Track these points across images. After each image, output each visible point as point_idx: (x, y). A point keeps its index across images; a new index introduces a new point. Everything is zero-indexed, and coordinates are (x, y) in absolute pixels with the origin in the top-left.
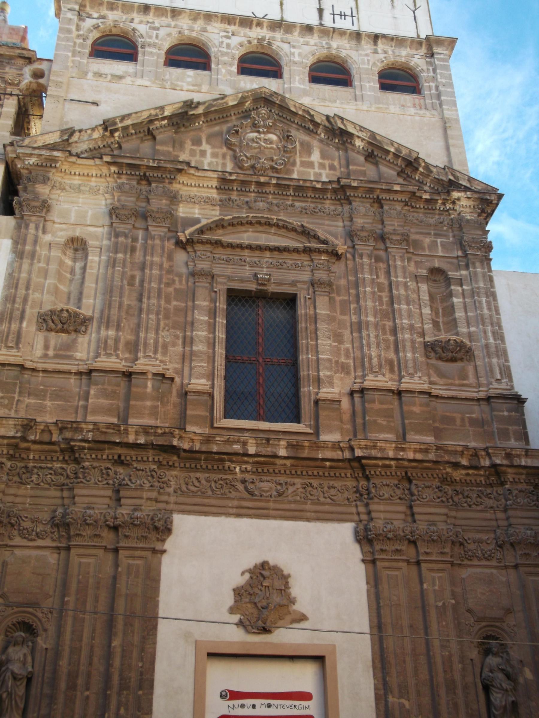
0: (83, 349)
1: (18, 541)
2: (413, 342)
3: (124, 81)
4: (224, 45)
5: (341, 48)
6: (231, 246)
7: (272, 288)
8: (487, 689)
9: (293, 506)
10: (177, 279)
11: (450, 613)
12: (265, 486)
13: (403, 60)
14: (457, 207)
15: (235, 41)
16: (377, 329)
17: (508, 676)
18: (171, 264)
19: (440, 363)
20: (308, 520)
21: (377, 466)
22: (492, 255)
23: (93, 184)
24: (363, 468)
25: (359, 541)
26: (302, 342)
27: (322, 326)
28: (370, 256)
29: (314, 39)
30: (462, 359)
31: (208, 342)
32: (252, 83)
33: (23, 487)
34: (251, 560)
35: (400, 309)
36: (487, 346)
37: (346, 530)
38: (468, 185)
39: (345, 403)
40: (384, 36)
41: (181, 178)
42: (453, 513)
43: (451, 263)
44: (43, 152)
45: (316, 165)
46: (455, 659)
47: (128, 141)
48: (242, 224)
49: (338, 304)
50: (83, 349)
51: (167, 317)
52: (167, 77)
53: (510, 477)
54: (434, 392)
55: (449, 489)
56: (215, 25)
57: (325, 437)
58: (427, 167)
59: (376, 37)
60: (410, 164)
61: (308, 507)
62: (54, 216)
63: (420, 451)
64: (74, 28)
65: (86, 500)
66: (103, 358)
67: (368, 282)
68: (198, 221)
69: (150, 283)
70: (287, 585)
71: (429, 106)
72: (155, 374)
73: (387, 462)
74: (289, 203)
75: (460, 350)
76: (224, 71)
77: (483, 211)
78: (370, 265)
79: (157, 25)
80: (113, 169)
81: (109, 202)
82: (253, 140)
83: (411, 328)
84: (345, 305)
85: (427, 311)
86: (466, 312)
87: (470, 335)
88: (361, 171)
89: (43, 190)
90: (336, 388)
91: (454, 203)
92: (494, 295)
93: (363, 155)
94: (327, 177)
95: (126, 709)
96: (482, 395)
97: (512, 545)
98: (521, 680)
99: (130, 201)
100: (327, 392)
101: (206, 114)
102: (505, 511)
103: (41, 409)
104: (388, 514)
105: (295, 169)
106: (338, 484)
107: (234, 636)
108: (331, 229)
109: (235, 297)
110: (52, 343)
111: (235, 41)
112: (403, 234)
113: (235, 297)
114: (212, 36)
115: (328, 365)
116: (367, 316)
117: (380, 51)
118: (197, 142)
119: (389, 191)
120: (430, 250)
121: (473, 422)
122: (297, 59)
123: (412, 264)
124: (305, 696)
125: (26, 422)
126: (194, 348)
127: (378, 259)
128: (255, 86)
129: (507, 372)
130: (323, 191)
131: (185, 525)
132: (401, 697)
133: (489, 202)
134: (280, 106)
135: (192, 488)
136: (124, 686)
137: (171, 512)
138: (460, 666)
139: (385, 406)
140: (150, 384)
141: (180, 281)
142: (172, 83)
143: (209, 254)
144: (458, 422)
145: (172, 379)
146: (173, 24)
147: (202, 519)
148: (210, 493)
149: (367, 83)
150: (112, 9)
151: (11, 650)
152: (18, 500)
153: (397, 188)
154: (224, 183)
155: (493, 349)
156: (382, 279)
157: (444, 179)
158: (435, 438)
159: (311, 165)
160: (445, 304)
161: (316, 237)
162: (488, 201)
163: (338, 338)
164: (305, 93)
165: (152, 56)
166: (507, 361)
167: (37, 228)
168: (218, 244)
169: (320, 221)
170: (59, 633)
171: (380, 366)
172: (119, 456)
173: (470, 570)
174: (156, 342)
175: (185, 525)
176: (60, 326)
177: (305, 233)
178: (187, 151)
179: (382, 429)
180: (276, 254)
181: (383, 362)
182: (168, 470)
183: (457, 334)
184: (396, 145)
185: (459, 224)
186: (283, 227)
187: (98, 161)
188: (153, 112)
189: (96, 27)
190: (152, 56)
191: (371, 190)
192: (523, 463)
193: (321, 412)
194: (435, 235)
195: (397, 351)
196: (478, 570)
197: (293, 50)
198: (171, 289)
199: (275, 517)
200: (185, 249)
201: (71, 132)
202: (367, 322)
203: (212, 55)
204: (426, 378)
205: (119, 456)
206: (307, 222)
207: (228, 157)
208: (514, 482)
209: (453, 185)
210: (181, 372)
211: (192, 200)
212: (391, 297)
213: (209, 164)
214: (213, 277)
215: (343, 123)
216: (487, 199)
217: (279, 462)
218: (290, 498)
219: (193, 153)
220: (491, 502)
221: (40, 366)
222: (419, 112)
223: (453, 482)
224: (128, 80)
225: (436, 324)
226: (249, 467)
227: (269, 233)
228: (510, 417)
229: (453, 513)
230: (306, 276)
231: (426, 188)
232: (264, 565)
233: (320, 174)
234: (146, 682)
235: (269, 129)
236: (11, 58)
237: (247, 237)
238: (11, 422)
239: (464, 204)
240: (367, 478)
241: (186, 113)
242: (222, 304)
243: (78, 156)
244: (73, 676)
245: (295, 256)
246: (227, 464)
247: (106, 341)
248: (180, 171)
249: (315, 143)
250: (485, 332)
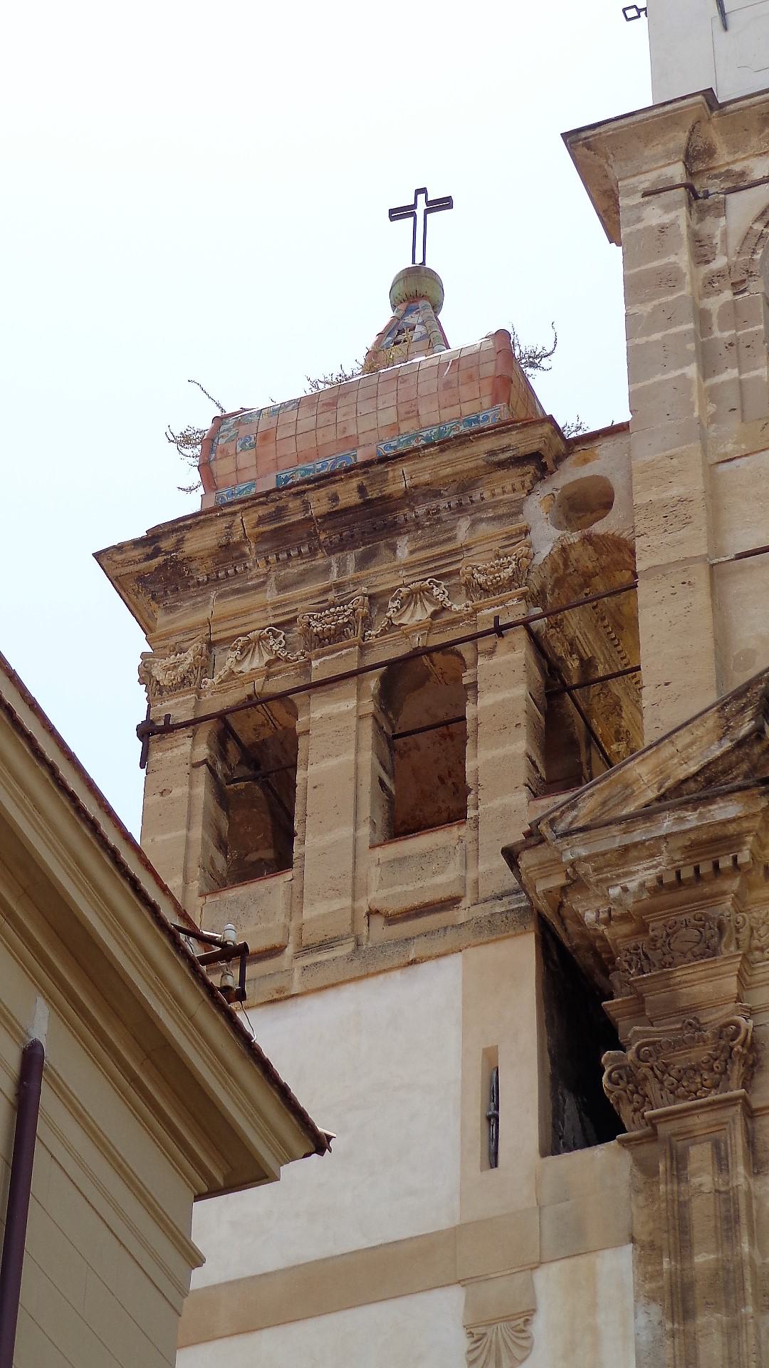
236: (465, 485)
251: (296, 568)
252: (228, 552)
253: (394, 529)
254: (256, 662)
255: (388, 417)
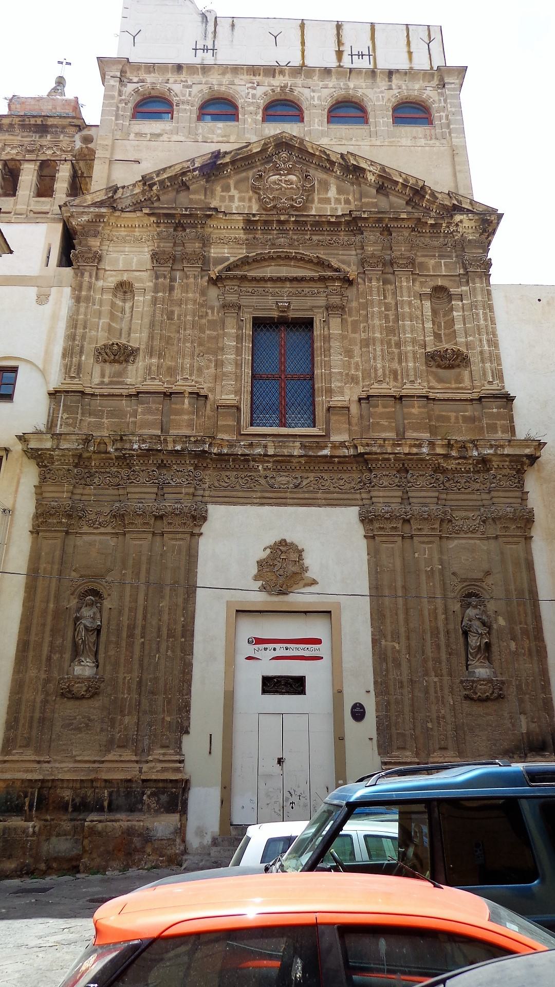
0: (135, 375)
1: (85, 529)
2: (414, 353)
3: (161, 139)
4: (250, 96)
5: (359, 88)
6: (254, 279)
7: (292, 315)
8: (466, 634)
9: (307, 495)
10: (209, 311)
11: (437, 576)
12: (283, 479)
13: (416, 93)
14: (460, 229)
15: (260, 91)
16: (382, 344)
17: (484, 624)
18: (204, 298)
19: (440, 370)
20: (319, 506)
21: (378, 460)
22: (492, 271)
23: (137, 234)
24: (366, 462)
25: (362, 521)
26: (317, 359)
27: (335, 344)
28: (378, 280)
29: (332, 82)
30: (459, 366)
31: (236, 364)
32: (273, 129)
33: (88, 487)
34: (272, 538)
35: (404, 325)
36: (481, 353)
37: (353, 513)
38: (470, 208)
39: (354, 409)
40: (397, 71)
41: (210, 222)
42: (444, 496)
43: (454, 281)
44: (92, 210)
45: (333, 200)
46: (440, 611)
47: (164, 193)
48: (265, 260)
49: (349, 324)
50: (135, 375)
51: (200, 344)
52: (200, 131)
53: (495, 464)
54: (431, 395)
55: (441, 477)
56: (242, 77)
57: (334, 438)
58: (433, 194)
59: (390, 73)
60: (417, 193)
61: (319, 495)
62: (106, 265)
63: (415, 446)
64: (116, 94)
65: (137, 496)
66: (148, 382)
67: (376, 302)
68: (227, 259)
69: (185, 316)
70: (300, 557)
71: (439, 136)
72: (190, 393)
73: (386, 456)
74: (307, 237)
75: (457, 358)
76: (250, 120)
77: (484, 231)
78: (378, 288)
79: (190, 83)
80: (153, 219)
81: (151, 248)
82: (275, 183)
83: (414, 341)
84: (355, 324)
85: (429, 325)
86: (465, 324)
87: (467, 345)
88: (372, 203)
89: (94, 243)
90: (347, 395)
91: (457, 225)
92: (491, 308)
93: (374, 187)
94: (342, 210)
95: (173, 652)
96: (475, 396)
97: (494, 519)
98: (495, 626)
99: (167, 246)
100: (337, 400)
101: (233, 162)
102: (489, 492)
103: (99, 426)
104: (386, 498)
105: (314, 206)
106: (345, 476)
107: (258, 599)
108: (345, 260)
109: (259, 324)
110: (107, 373)
111: (260, 91)
112: (408, 258)
113: (259, 324)
114: (238, 88)
115: (339, 377)
116: (374, 333)
117: (394, 87)
118: (226, 188)
119: (397, 219)
120: (434, 271)
121: (465, 419)
122: (316, 102)
123: (417, 284)
124: (318, 641)
125: (84, 437)
126: (225, 370)
127: (386, 282)
128: (273, 133)
129: (499, 375)
130: (338, 224)
131: (217, 513)
132: (393, 641)
133: (489, 222)
134: (300, 150)
135: (224, 484)
136: (171, 634)
137: (206, 503)
138: (443, 616)
139: (388, 410)
140: (186, 401)
141: (213, 313)
142: (203, 136)
143: (236, 288)
144: (453, 420)
145: (206, 397)
146: (204, 80)
147: (232, 508)
148: (238, 487)
149: (381, 118)
150: (150, 72)
151: (83, 610)
152: (84, 498)
153: (404, 216)
154: (250, 223)
155: (487, 355)
156: (389, 300)
157: (448, 204)
158: (430, 433)
159: (328, 201)
160: (447, 318)
161: (330, 266)
162: (488, 221)
163: (349, 353)
164: (323, 134)
165: (186, 113)
166: (499, 364)
167: (91, 276)
168: (244, 278)
169: (336, 252)
170: (121, 597)
171: (384, 374)
172: (162, 461)
173: (456, 542)
174: (192, 366)
175: (217, 513)
176: (112, 357)
177: (321, 263)
178: (218, 198)
179: (384, 429)
180: (295, 284)
181: (387, 372)
182: (203, 470)
183: (456, 344)
184: (404, 176)
185: (461, 245)
186: (302, 260)
187: (139, 214)
188: (185, 165)
189: (137, 91)
190: (186, 113)
191: (380, 220)
192: (506, 453)
193: (332, 417)
194: (439, 256)
195: (400, 362)
196: (464, 541)
197: (312, 94)
198: (204, 321)
199: (292, 505)
200: (216, 285)
201: (115, 189)
202: (374, 339)
203: (240, 106)
204: (425, 384)
205: (162, 461)
206: (322, 254)
207: (254, 200)
208: (499, 468)
209: (457, 209)
210: (212, 390)
211: (222, 242)
212: (397, 316)
213: (237, 208)
214: (240, 308)
215: (355, 159)
216: (487, 220)
217: (295, 460)
218: (305, 489)
219: (222, 199)
220: (477, 486)
221: (97, 391)
222: (429, 142)
223: (444, 471)
224: (165, 137)
225: (437, 336)
226: (270, 465)
227: (290, 266)
228: (498, 413)
229: (444, 496)
230: (322, 301)
231: (433, 214)
232: (283, 542)
233: (336, 209)
234: (188, 632)
235: (290, 172)
236: (64, 127)
237: (270, 271)
238: (73, 437)
239: (466, 224)
240: (370, 470)
241: (215, 163)
242: (248, 331)
243: (122, 211)
244: (132, 628)
245: (312, 284)
246: (252, 463)
247: (150, 368)
248: (210, 216)
249: (332, 180)
250: (481, 340)
251: (26, 134)
252: (11, 125)
253: (47, 132)
254: (14, 151)
255: (50, 107)
